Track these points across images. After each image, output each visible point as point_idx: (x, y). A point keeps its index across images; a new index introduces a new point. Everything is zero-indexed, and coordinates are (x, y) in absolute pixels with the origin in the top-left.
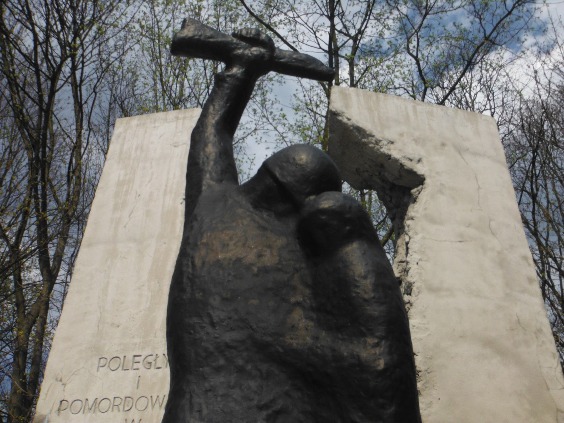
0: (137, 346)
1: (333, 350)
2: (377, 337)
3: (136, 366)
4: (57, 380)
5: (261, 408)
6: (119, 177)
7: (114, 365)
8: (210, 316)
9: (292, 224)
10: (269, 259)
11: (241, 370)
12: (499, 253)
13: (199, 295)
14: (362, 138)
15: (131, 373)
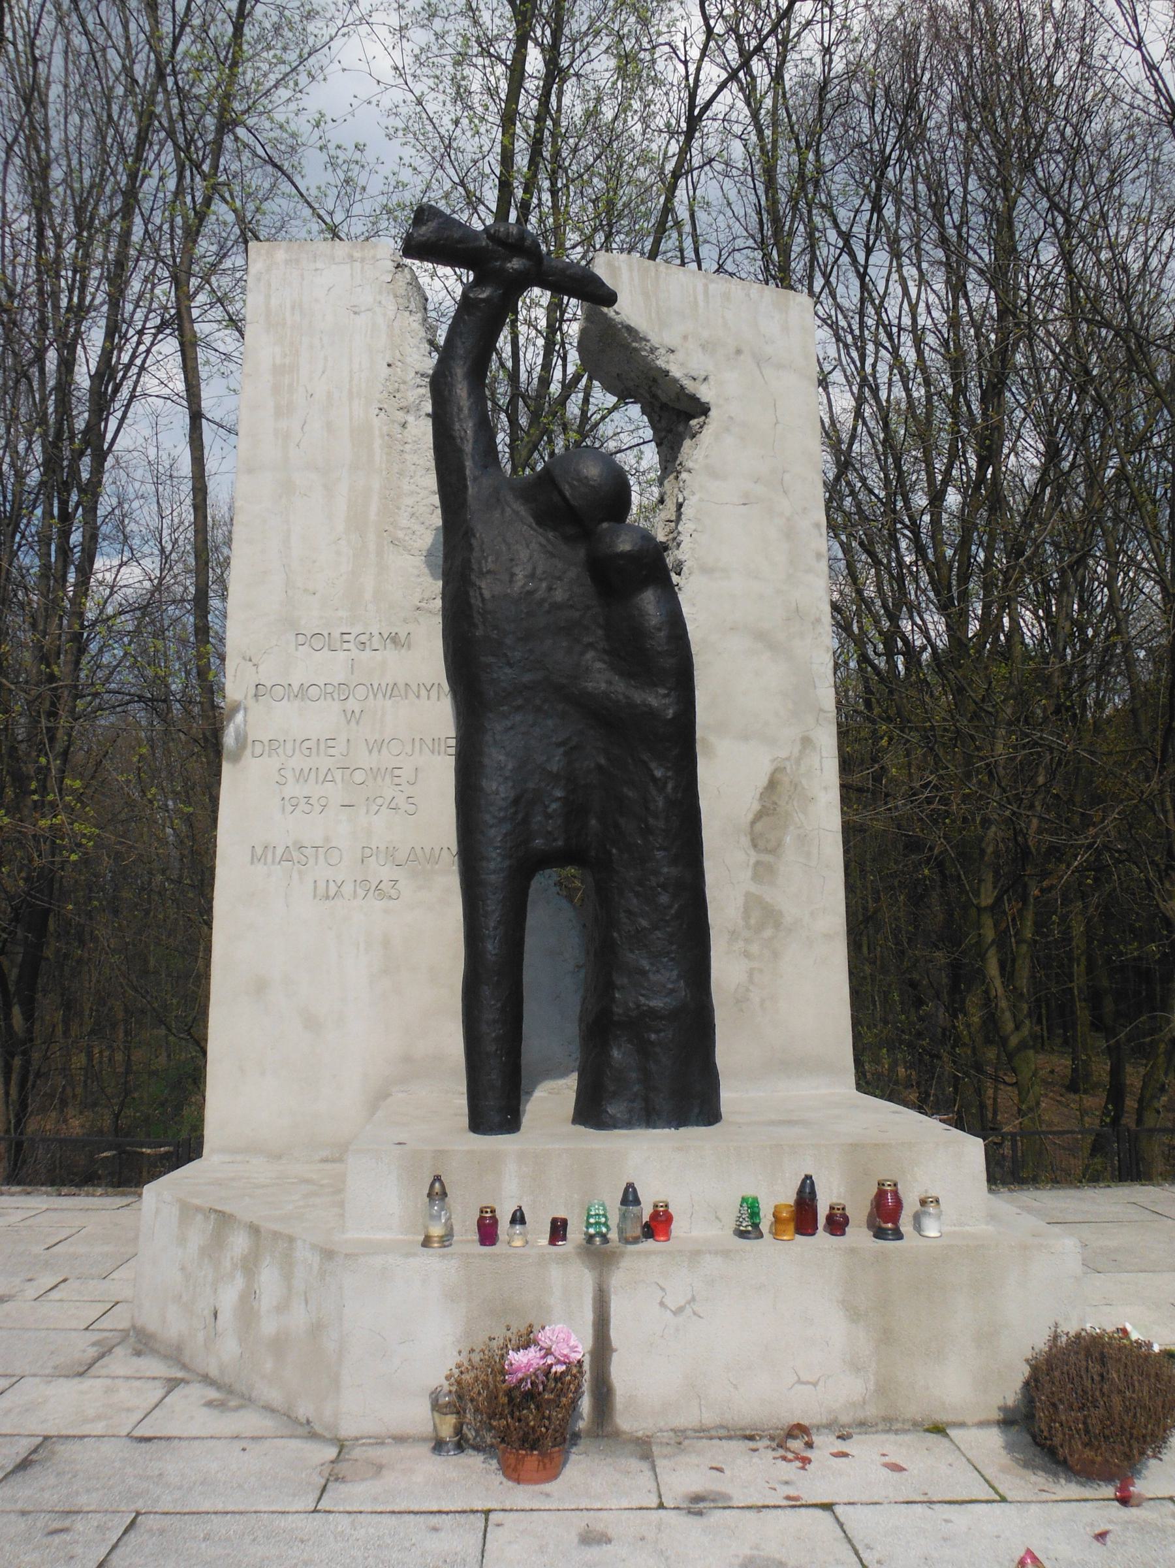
1: (627, 697)
3: (346, 646)
5: (559, 745)
8: (505, 655)
9: (581, 553)
10: (559, 595)
12: (788, 519)
13: (494, 635)
15: (342, 655)
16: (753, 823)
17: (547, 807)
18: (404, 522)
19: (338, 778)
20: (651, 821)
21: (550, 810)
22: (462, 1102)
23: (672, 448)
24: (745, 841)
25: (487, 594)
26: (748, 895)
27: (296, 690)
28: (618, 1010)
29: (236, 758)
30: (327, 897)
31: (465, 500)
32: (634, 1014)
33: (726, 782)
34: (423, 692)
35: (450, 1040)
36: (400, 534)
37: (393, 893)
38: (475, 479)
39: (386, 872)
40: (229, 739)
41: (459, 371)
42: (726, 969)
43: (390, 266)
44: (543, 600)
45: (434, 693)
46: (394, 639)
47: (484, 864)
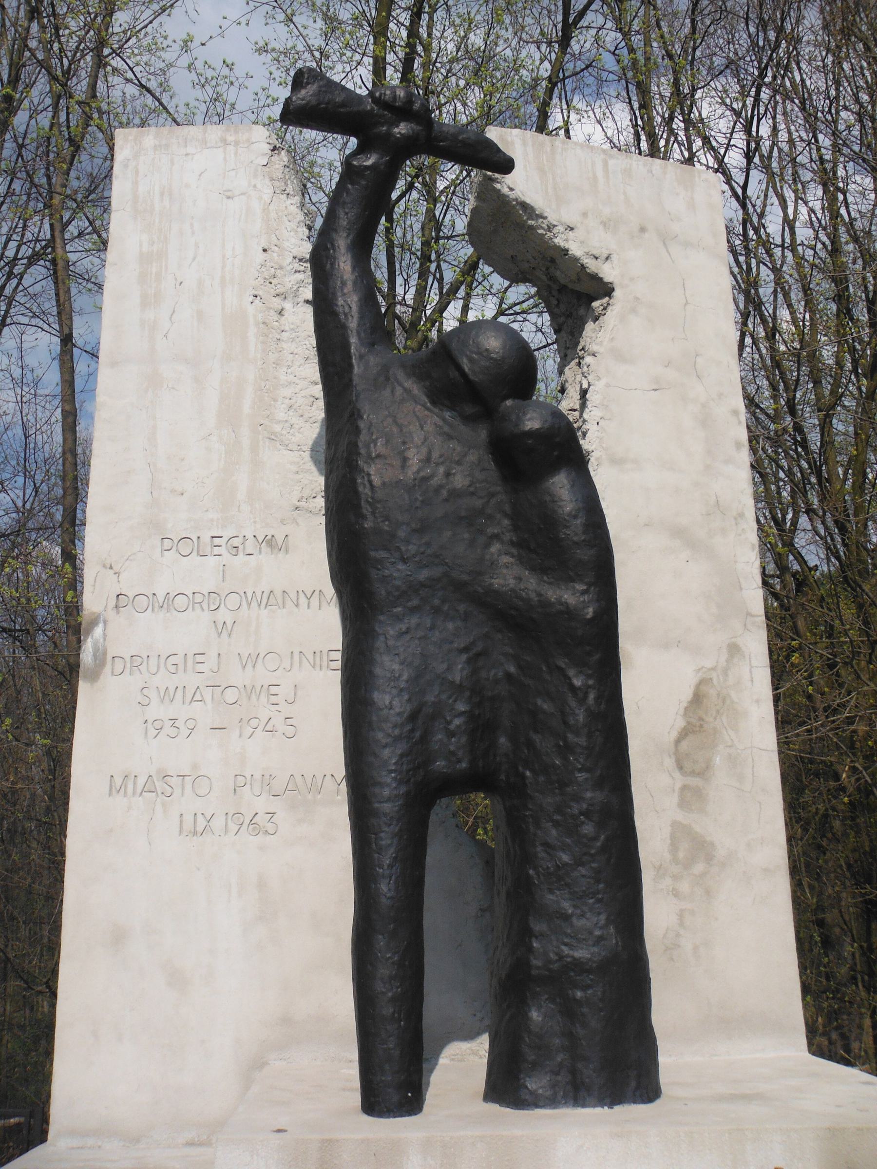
0: (215, 523)
1: (539, 595)
2: (586, 584)
3: (216, 550)
4: (104, 566)
5: (466, 650)
6: (141, 246)
7: (185, 548)
9: (483, 434)
10: (460, 481)
11: (436, 611)
13: (386, 526)
14: (528, 219)
15: (212, 561)
16: (678, 742)
17: (449, 723)
18: (281, 415)
19: (208, 698)
20: (570, 737)
21: (452, 727)
22: (352, 1072)
23: (572, 334)
24: (669, 762)
25: (376, 480)
26: (675, 825)
27: (161, 600)
28: (536, 962)
29: (95, 676)
30: (195, 833)
31: (351, 380)
32: (555, 966)
33: (651, 691)
34: (303, 600)
35: (336, 998)
36: (277, 428)
37: (270, 827)
38: (361, 357)
39: (262, 804)
40: (87, 656)
41: (342, 242)
42: (658, 914)
43: (267, 148)
44: (441, 487)
45: (315, 601)
46: (270, 542)
47: (377, 790)
